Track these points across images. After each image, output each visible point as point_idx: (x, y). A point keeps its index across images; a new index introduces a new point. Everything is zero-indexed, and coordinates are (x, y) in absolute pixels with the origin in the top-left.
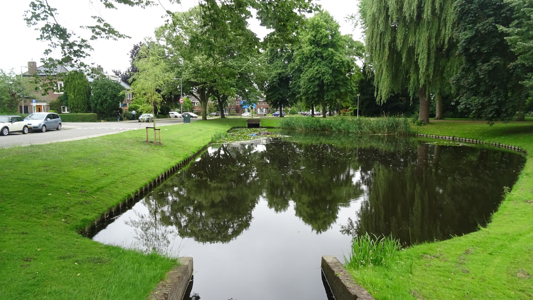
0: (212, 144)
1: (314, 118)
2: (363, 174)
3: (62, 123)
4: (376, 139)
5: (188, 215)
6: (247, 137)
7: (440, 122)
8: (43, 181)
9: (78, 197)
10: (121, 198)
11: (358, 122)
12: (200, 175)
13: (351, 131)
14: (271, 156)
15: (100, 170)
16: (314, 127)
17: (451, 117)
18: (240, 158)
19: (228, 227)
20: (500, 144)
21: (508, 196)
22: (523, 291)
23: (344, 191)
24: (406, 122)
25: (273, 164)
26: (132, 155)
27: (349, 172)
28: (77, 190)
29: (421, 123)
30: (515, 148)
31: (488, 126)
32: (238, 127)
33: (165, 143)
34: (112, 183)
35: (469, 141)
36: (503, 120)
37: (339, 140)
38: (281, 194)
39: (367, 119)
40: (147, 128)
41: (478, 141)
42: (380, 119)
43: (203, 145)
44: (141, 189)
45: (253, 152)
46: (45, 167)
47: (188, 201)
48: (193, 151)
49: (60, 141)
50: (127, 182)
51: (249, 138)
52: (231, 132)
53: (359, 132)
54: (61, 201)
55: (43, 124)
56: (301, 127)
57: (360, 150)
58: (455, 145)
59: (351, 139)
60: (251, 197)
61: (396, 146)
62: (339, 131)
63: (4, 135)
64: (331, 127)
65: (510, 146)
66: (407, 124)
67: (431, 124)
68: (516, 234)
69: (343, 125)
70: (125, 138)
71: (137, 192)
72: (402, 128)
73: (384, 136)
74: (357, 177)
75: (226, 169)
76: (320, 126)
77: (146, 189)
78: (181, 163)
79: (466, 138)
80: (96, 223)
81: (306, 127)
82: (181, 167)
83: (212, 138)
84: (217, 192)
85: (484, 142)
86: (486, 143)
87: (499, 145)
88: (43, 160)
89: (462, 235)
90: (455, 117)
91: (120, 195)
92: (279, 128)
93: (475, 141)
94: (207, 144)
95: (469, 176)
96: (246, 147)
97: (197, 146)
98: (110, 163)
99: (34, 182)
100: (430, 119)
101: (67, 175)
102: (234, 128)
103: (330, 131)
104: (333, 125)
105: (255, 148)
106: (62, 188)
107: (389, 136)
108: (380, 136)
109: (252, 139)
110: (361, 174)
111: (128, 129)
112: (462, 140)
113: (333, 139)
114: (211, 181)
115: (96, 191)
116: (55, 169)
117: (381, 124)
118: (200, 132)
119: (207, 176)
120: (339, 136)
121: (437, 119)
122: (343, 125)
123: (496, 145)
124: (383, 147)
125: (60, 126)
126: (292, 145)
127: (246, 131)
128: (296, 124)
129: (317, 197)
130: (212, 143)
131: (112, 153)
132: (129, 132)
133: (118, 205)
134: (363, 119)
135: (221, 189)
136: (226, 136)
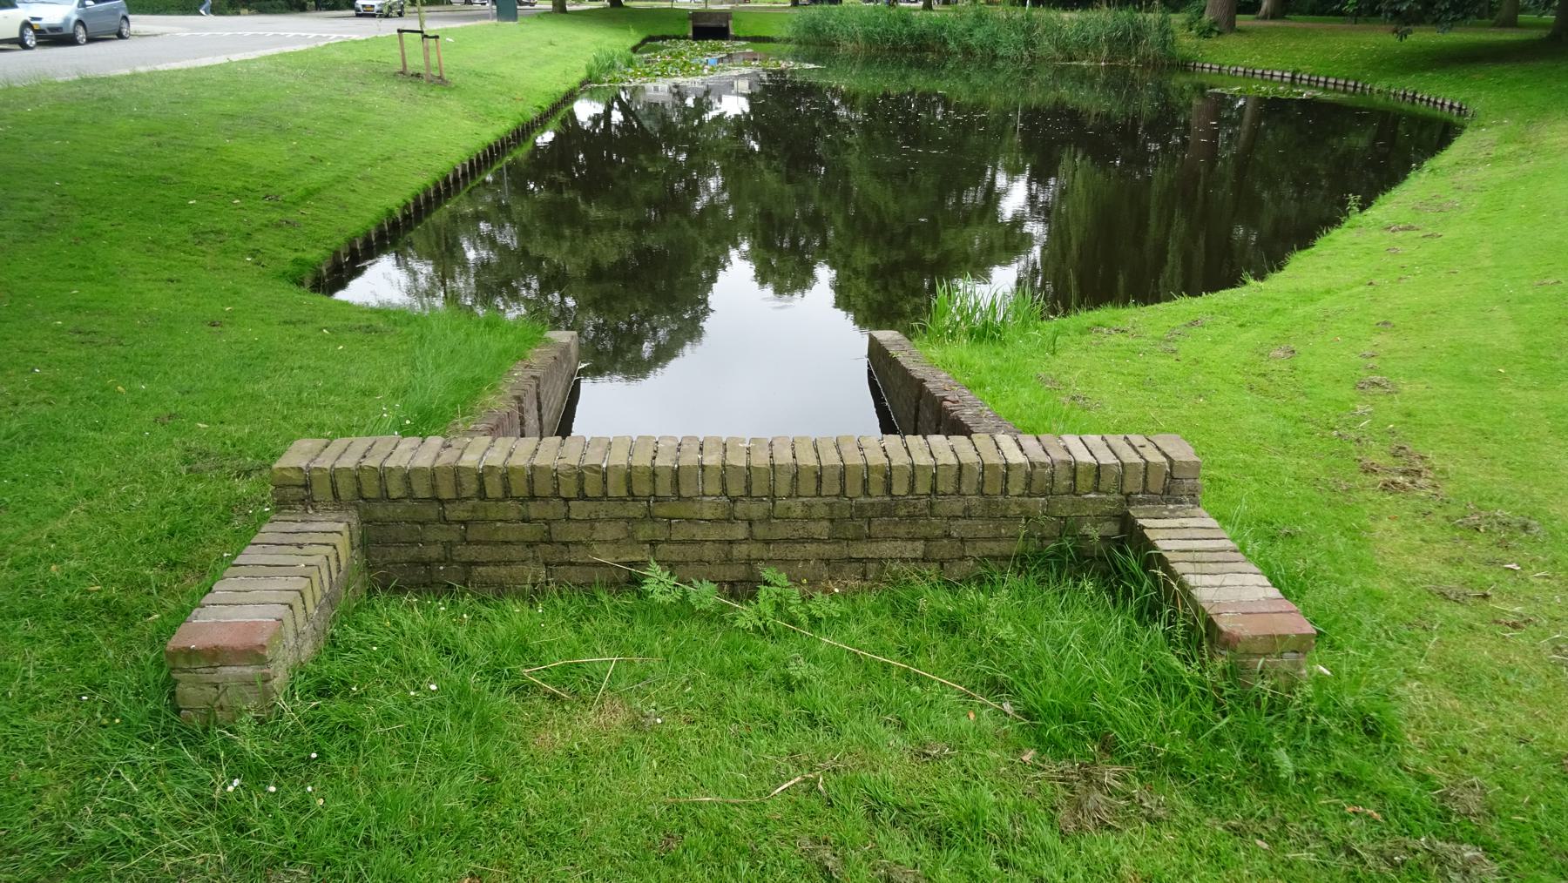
0: (589, 86)
1: (894, 12)
2: (1034, 186)
3: (130, 17)
4: (1073, 78)
5: (527, 301)
6: (691, 66)
7: (1269, 27)
8: (163, 170)
9: (265, 211)
10: (371, 216)
11: (1026, 24)
12: (552, 185)
13: (1001, 51)
14: (763, 130)
15: (296, 148)
16: (892, 37)
17: (1312, 13)
18: (670, 134)
19: (638, 340)
20: (1415, 93)
21: (1356, 217)
22: (1265, 375)
23: (976, 238)
24: (1166, 26)
25: (770, 157)
26: (371, 110)
27: (993, 182)
28: (256, 194)
29: (1211, 30)
30: (1451, 107)
31: (1392, 39)
32: (664, 38)
33: (456, 79)
34: (339, 180)
35: (1335, 84)
36: (1436, 22)
37: (968, 78)
38: (794, 242)
39: (1053, 14)
40: (400, 31)
41: (1360, 85)
42: (1092, 15)
43: (564, 88)
44: (416, 199)
45: (708, 117)
46: (149, 135)
47: (527, 261)
48: (539, 103)
49: (160, 68)
50: (377, 180)
51: (698, 68)
52: (641, 52)
53: (1026, 53)
54: (225, 218)
55: (75, 17)
56: (854, 39)
57: (1033, 115)
58: (1291, 96)
59: (1001, 78)
60: (705, 250)
61: (1129, 98)
62: (968, 51)
63: (79, 44)
64: (945, 40)
65: (1440, 101)
66: (1166, 33)
67: (1241, 31)
68: (1321, 290)
69: (979, 34)
70: (337, 63)
71: (407, 206)
72: (1152, 46)
73: (1098, 70)
74: (1015, 197)
75: (630, 167)
76: (911, 36)
77: (394, 225)
78: (510, 136)
79: (1327, 78)
80: (324, 269)
81: (868, 37)
82: (509, 146)
83: (590, 69)
84: (605, 237)
85: (1376, 89)
86: (1379, 92)
87: (1414, 97)
88: (137, 118)
89: (1201, 295)
90: (1322, 14)
91: (368, 210)
92: (788, 41)
93: (1352, 83)
94: (577, 85)
95: (1321, 188)
96: (690, 102)
97: (547, 89)
98: (317, 130)
99: (139, 173)
100: (1238, 16)
101: (215, 157)
102: (652, 39)
103: (939, 52)
104: (950, 32)
105: (716, 104)
106: (216, 189)
107: (1109, 69)
108: (1084, 70)
109: (706, 71)
110: (1030, 189)
111: (334, 38)
112: (1318, 81)
113: (947, 77)
114: (588, 202)
115: (303, 199)
116: (180, 142)
117: (1091, 33)
118: (550, 50)
119: (574, 184)
120: (965, 67)
121: (1265, 18)
122: (979, 34)
123: (1405, 95)
124: (1091, 101)
125: (125, 25)
126: (828, 94)
127: (689, 49)
128: (841, 27)
129: (899, 255)
130: (588, 86)
131: (313, 102)
132: (278, 63)
133: (368, 234)
134: (1041, 13)
135: (615, 225)
136: (630, 63)
